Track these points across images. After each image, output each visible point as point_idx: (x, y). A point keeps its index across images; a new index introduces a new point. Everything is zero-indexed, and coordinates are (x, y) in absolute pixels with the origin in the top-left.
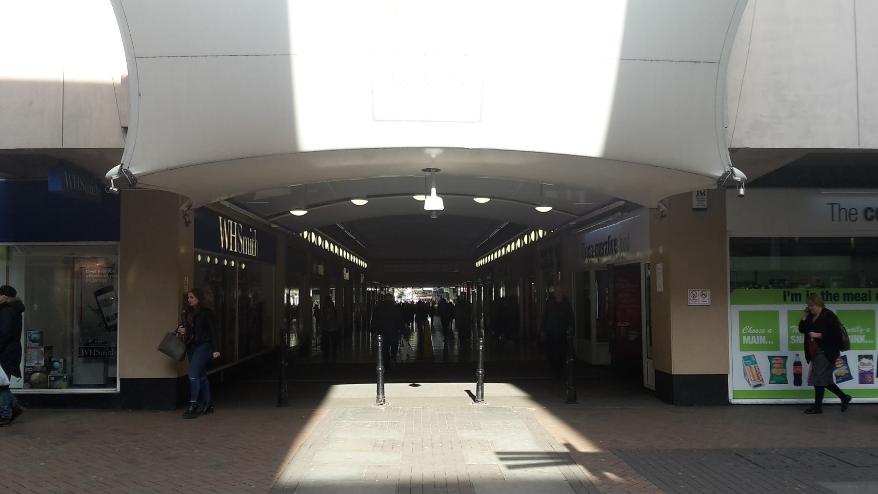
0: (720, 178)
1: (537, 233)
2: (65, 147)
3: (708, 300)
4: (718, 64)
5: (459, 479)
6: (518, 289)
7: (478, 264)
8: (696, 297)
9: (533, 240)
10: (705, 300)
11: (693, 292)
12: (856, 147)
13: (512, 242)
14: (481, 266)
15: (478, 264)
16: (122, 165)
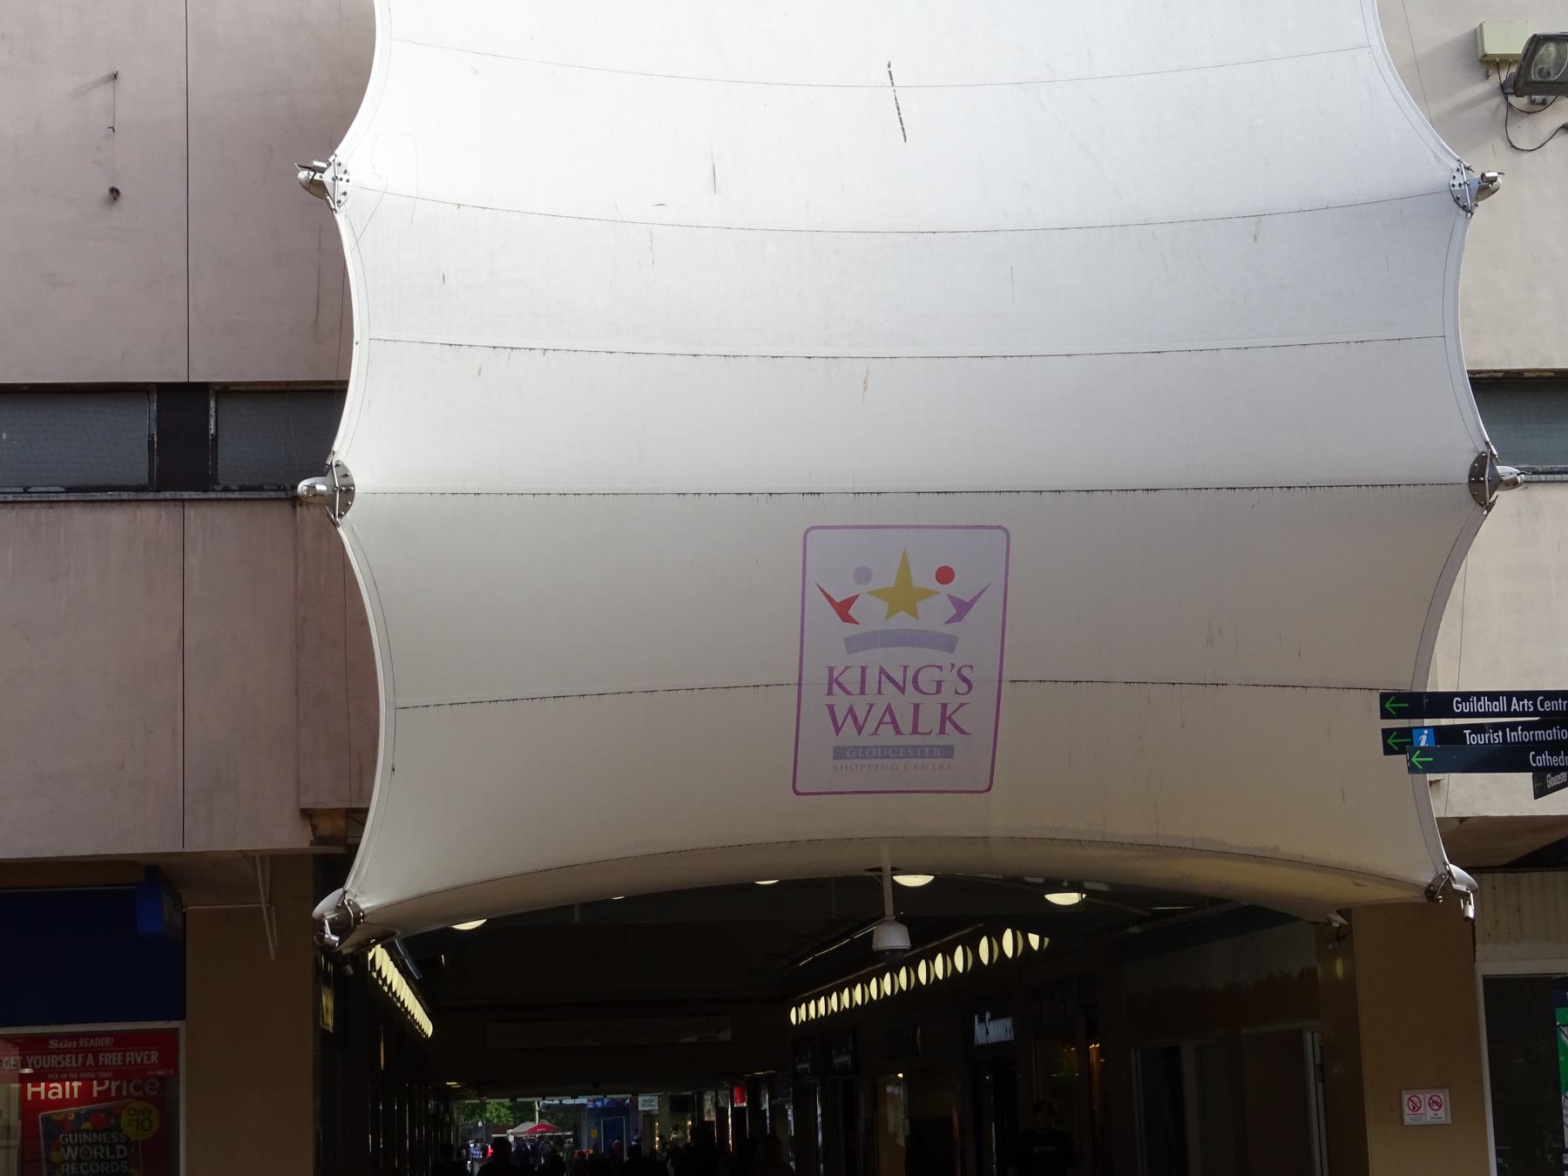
0: (1430, 885)
1: (865, 986)
2: (188, 849)
3: (1446, 1114)
5: (1497, 71)
7: (797, 1015)
8: (1419, 1108)
9: (904, 987)
13: (832, 993)
15: (797, 1015)
16: (345, 892)
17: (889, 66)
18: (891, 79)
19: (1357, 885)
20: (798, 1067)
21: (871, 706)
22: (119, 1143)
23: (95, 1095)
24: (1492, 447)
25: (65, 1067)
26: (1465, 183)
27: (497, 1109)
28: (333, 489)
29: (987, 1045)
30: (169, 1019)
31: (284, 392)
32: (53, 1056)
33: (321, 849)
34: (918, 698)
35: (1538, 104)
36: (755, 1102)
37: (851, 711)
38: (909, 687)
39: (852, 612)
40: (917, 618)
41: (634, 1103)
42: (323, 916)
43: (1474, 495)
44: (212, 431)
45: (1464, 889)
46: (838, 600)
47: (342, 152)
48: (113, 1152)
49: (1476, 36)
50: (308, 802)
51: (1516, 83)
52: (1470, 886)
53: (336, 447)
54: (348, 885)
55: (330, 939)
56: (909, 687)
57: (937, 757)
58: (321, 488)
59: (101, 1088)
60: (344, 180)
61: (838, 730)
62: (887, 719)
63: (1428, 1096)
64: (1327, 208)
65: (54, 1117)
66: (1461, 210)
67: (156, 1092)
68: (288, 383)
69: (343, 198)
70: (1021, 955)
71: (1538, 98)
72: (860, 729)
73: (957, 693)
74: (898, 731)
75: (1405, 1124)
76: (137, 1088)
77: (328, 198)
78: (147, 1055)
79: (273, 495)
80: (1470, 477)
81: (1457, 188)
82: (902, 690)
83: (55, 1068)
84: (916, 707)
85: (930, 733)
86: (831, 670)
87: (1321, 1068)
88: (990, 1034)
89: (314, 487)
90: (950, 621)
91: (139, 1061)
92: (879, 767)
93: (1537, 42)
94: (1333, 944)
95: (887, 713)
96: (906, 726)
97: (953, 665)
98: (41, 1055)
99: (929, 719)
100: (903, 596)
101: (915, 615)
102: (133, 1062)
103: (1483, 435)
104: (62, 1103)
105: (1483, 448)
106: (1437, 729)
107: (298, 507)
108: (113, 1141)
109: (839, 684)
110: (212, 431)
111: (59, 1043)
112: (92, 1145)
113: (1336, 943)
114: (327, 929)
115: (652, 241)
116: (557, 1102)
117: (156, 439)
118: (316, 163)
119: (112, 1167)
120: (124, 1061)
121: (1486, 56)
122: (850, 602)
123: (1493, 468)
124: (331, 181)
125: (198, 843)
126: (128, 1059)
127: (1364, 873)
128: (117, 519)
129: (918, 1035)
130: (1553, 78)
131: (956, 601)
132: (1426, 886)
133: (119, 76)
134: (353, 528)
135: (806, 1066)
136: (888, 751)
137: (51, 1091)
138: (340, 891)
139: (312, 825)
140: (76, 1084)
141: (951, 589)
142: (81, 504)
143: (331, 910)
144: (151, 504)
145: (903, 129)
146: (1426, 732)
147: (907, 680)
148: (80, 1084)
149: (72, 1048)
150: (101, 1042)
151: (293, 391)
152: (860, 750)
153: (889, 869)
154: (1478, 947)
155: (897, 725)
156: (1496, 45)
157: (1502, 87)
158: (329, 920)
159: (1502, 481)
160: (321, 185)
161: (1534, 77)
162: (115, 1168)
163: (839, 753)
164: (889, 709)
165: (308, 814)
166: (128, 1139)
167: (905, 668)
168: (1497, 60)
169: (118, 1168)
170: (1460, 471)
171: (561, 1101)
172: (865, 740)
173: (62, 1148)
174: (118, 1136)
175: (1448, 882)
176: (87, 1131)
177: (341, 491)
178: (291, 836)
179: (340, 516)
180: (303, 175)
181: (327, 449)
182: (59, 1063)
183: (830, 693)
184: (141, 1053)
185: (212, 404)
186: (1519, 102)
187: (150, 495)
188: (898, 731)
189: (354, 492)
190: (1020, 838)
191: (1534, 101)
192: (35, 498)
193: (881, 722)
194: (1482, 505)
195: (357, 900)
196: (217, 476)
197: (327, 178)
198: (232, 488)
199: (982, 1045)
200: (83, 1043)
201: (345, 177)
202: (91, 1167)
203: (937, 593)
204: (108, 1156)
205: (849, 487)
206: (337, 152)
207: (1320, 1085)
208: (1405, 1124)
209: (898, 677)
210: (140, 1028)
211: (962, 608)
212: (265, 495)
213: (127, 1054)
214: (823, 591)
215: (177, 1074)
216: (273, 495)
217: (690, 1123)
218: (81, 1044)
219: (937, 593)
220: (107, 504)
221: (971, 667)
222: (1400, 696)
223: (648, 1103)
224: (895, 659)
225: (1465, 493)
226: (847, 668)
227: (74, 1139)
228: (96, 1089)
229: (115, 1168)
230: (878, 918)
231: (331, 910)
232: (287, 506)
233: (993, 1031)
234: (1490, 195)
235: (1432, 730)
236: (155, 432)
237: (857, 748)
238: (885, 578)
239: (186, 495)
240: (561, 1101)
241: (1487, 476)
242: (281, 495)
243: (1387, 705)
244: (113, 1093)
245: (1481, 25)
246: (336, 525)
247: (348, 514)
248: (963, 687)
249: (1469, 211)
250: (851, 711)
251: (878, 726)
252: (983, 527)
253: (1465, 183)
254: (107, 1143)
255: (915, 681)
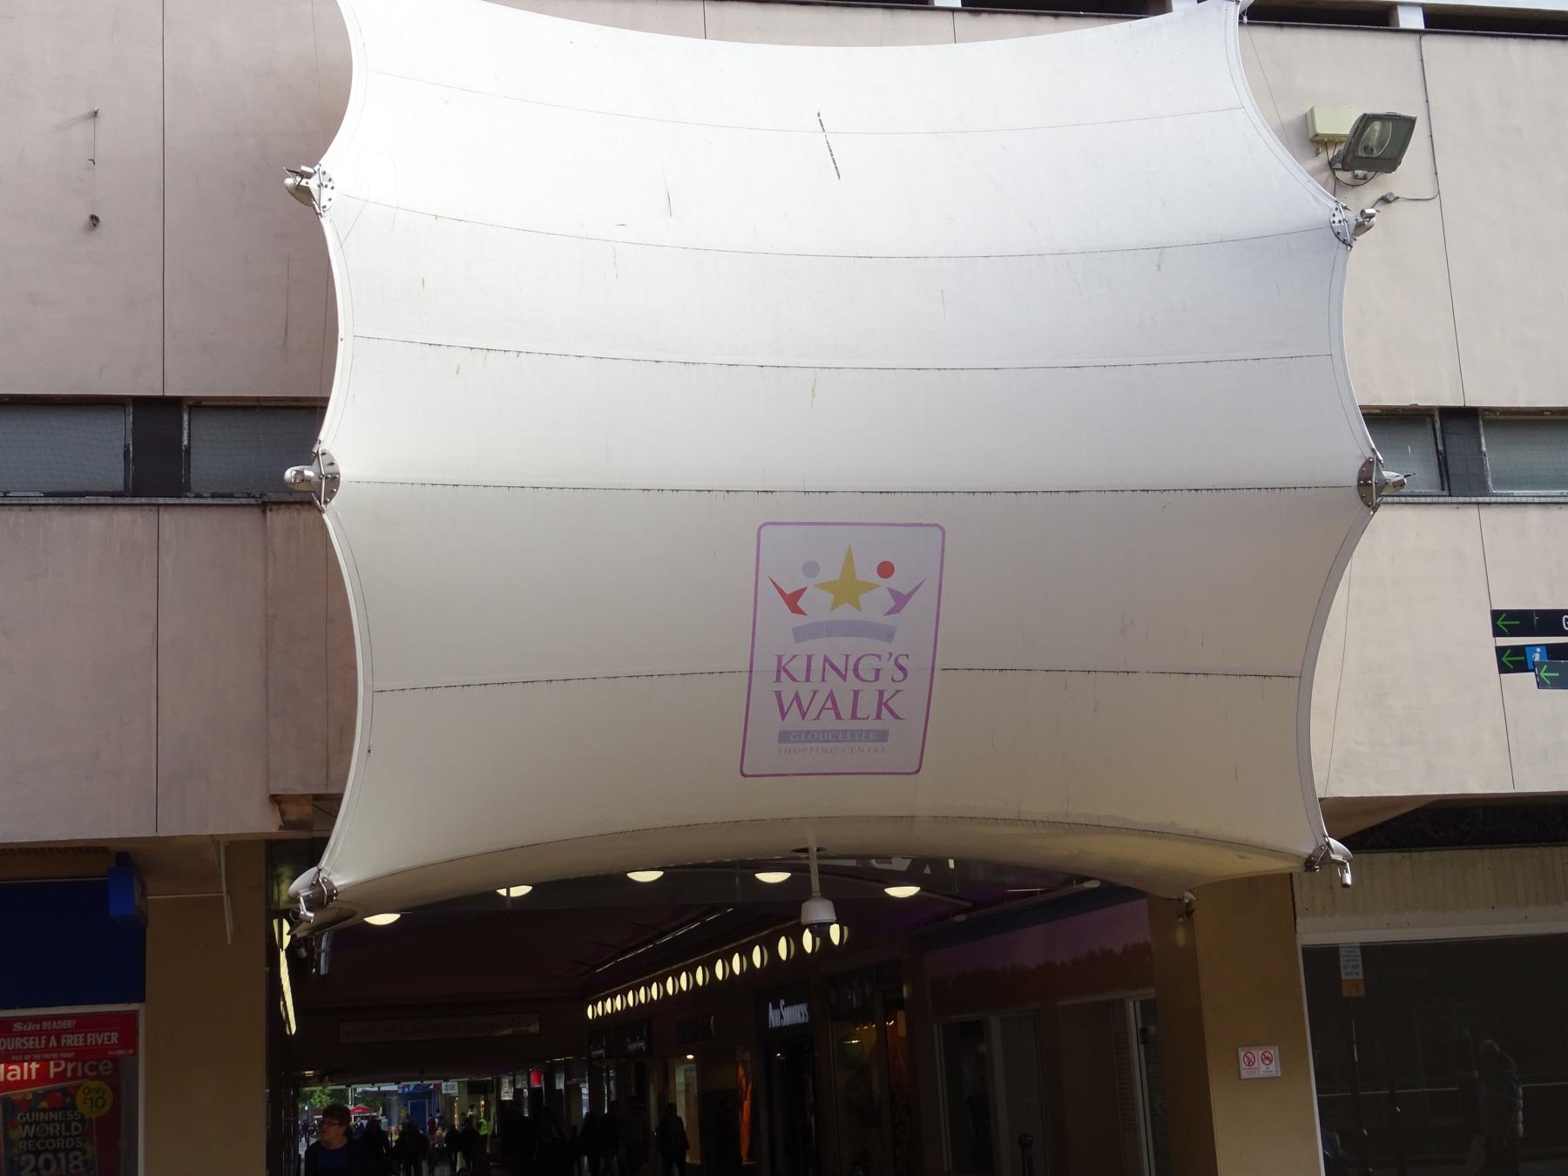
0: (1310, 856)
2: (161, 834)
4: (1298, 679)
6: (1353, 1024)
8: (1253, 1063)
10: (1271, 1069)
11: (1248, 1055)
12: (1511, 790)
13: (640, 988)
14: (598, 1020)
16: (320, 870)
17: (819, 115)
18: (822, 126)
19: (1241, 857)
20: (593, 1053)
21: (815, 692)
22: (74, 1120)
23: (52, 1076)
24: (1378, 453)
25: (28, 1049)
26: (1344, 220)
27: (319, 1096)
28: (320, 476)
29: (781, 1028)
30: (129, 1002)
31: (254, 407)
32: (17, 1039)
33: (289, 834)
34: (857, 685)
35: (1361, 179)
36: (550, 1082)
37: (797, 698)
38: (850, 675)
39: (800, 603)
40: (859, 610)
41: (438, 1087)
42: (298, 894)
43: (1362, 497)
44: (186, 442)
45: (1340, 858)
46: (788, 591)
47: (326, 162)
48: (68, 1129)
49: (1308, 120)
50: (277, 789)
51: (1345, 158)
52: (1345, 856)
53: (322, 436)
54: (323, 864)
55: (305, 915)
56: (850, 675)
57: (874, 741)
58: (309, 473)
59: (56, 1070)
60: (329, 187)
61: (783, 715)
62: (829, 704)
63: (1261, 1052)
64: (1221, 242)
65: (12, 1098)
66: (1341, 243)
67: (110, 1072)
68: (258, 399)
69: (328, 204)
70: (819, 949)
71: (1360, 173)
72: (804, 715)
73: (893, 680)
74: (838, 716)
75: (1243, 1077)
76: (92, 1069)
77: (314, 203)
78: (108, 1036)
79: (244, 501)
80: (1359, 481)
81: (1337, 224)
82: (844, 677)
83: (18, 1050)
84: (856, 693)
85: (867, 718)
86: (780, 658)
87: (1144, 1031)
88: (784, 1017)
89: (303, 472)
90: (889, 613)
91: (100, 1042)
92: (820, 750)
93: (1366, 120)
94: (1184, 918)
95: (829, 700)
96: (846, 711)
97: (891, 654)
98: (6, 1037)
99: (868, 705)
100: (847, 589)
101: (858, 608)
102: (94, 1043)
103: (1369, 442)
104: (21, 1084)
105: (1369, 454)
106: (1549, 647)
107: (268, 513)
108: (69, 1119)
109: (786, 671)
110: (186, 442)
111: (23, 1026)
112: (48, 1123)
113: (1186, 918)
114: (303, 905)
115: (615, 256)
116: (376, 1089)
117: (131, 449)
118: (304, 168)
119: (67, 1143)
120: (85, 1041)
121: (1317, 135)
122: (799, 593)
123: (1379, 471)
124: (317, 188)
125: (173, 826)
126: (89, 1040)
127: (1251, 846)
128: (94, 522)
129: (712, 1022)
130: (1376, 154)
131: (895, 594)
132: (1307, 857)
133: (99, 114)
134: (337, 514)
135: (600, 1052)
136: (828, 735)
137: (10, 1074)
138: (314, 869)
139: (280, 811)
140: (34, 1066)
141: (893, 582)
142: (59, 507)
143: (306, 888)
144: (127, 508)
145: (836, 168)
146: (1538, 650)
147: (849, 668)
148: (38, 1066)
149: (35, 1030)
150: (63, 1024)
151: (261, 407)
152: (803, 735)
153: (815, 849)
154: (1298, 921)
155: (838, 711)
156: (1324, 127)
157: (1330, 163)
158: (304, 897)
159: (1387, 483)
160: (307, 191)
161: (1361, 153)
162: (70, 1143)
163: (784, 737)
164: (831, 696)
165: (276, 800)
166: (83, 1116)
167: (847, 656)
168: (1326, 140)
169: (73, 1144)
170: (1349, 474)
171: (379, 1088)
172: (808, 725)
173: (20, 1127)
174: (73, 1113)
175: (1327, 853)
176: (44, 1110)
177: (327, 478)
178: (262, 822)
179: (326, 502)
180: (289, 181)
181: (313, 437)
182: (23, 1044)
183: (778, 680)
184: (102, 1035)
185: (186, 417)
186: (1345, 176)
187: (127, 500)
188: (838, 716)
189: (339, 480)
190: (943, 817)
191: (1357, 176)
192: (15, 501)
193: (823, 708)
194: (1369, 506)
195: (331, 878)
196: (189, 483)
197: (312, 184)
198: (205, 495)
199: (776, 1028)
200: (46, 1025)
201: (330, 185)
202: (47, 1144)
203: (878, 586)
204: (63, 1133)
205: (800, 486)
206: (321, 162)
207: (1142, 1046)
208: (1243, 1077)
209: (841, 665)
210: (85, 1011)
211: (901, 601)
212: (236, 501)
213: (89, 1035)
214: (774, 583)
215: (136, 1054)
216: (244, 501)
217: (483, 1103)
218: (44, 1027)
219: (878, 586)
220: (85, 508)
221: (907, 656)
222: (1512, 614)
223: (451, 1087)
224: (838, 648)
225: (1354, 495)
226: (794, 656)
227: (31, 1117)
228: (52, 1070)
229: (70, 1143)
230: (808, 896)
231: (306, 888)
232: (257, 512)
233: (790, 1015)
234: (1365, 231)
235: (1544, 647)
236: (131, 443)
237: (801, 732)
238: (831, 572)
239: (161, 500)
240: (379, 1088)
241: (1374, 480)
242: (252, 501)
243: (1499, 623)
244: (69, 1075)
245: (1312, 110)
246: (321, 511)
247: (333, 501)
248: (899, 675)
249: (1349, 245)
250: (797, 698)
251: (821, 711)
252: (921, 525)
253: (1344, 220)
254: (62, 1121)
255: (856, 670)
